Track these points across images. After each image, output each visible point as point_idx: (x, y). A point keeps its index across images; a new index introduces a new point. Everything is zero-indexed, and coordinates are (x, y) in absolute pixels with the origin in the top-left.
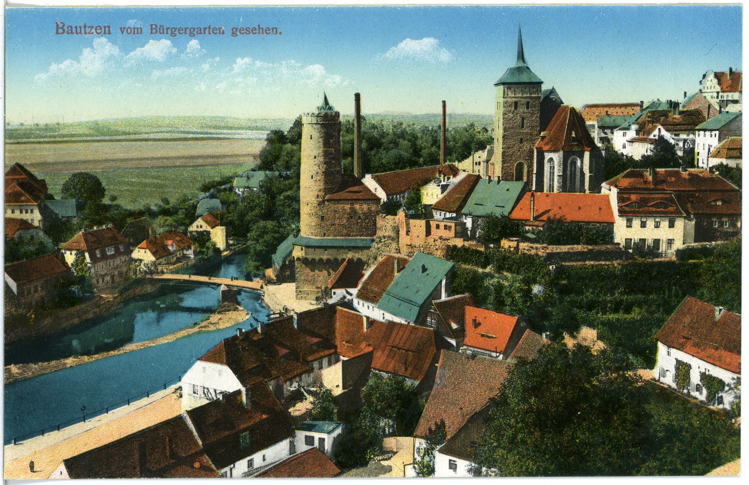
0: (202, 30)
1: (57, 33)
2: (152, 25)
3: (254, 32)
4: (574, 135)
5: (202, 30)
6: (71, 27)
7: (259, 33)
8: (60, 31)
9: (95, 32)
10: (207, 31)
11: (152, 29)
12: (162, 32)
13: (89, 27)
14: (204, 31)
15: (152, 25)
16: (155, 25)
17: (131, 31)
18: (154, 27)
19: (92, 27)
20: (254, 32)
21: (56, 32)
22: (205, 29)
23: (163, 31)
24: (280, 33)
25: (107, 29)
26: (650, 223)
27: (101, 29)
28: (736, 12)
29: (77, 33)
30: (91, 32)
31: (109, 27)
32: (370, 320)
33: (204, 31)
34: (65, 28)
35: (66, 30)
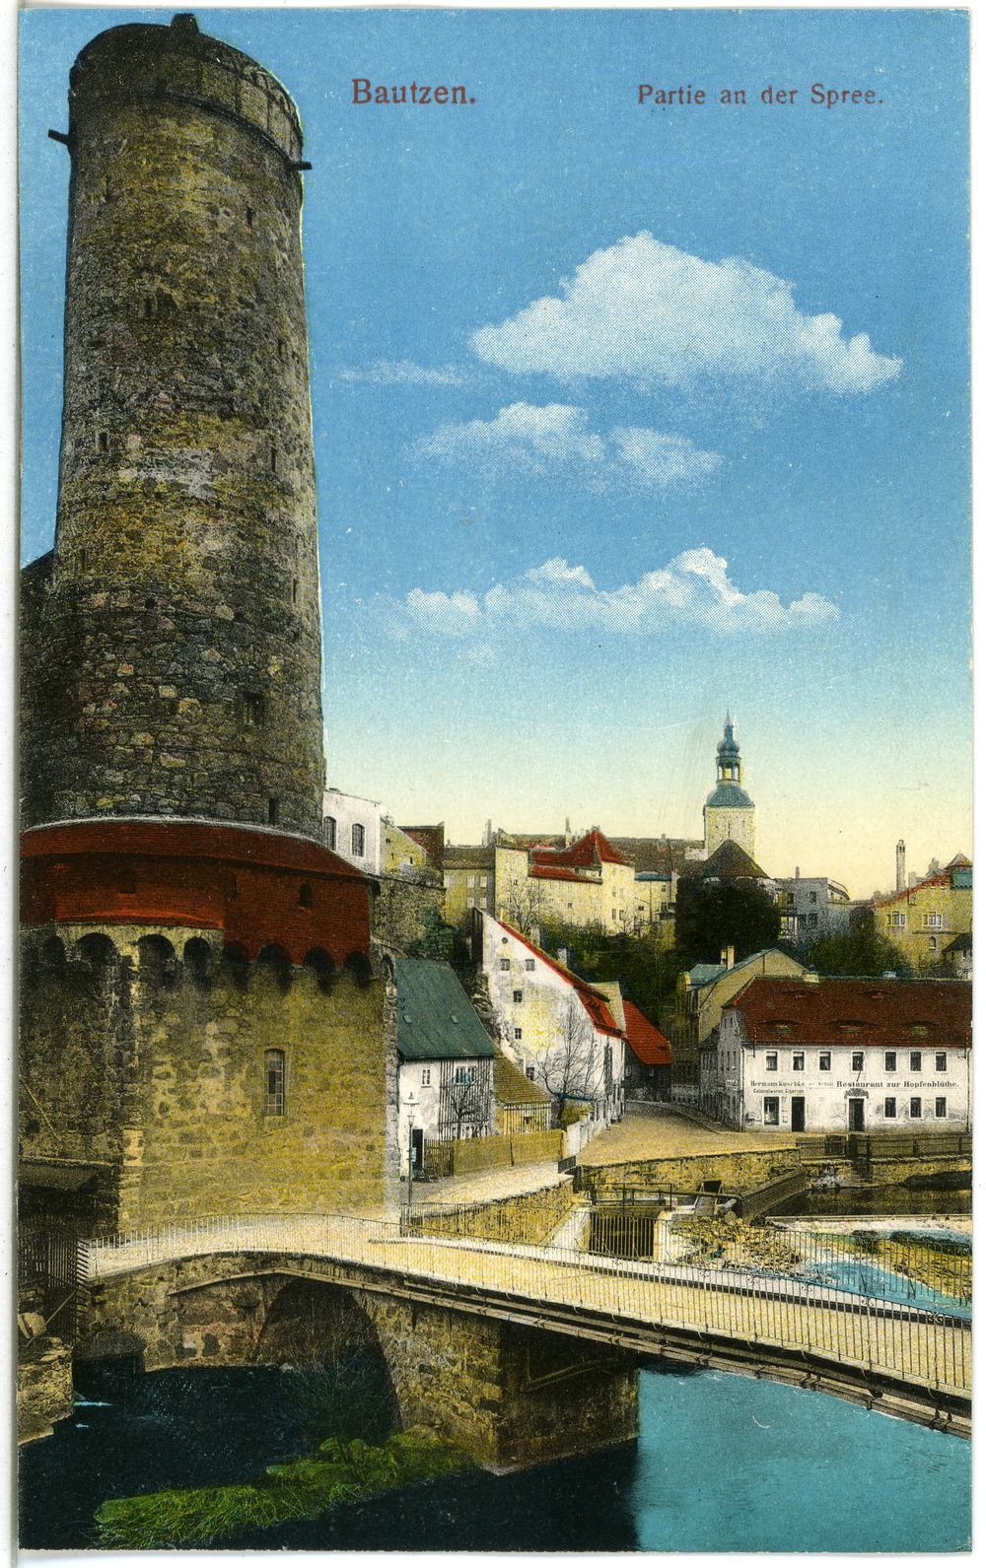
0: (667, 97)
1: (356, 101)
2: (356, 81)
3: (442, 97)
4: (350, 530)
5: (667, 97)
6: (384, 89)
7: (455, 101)
8: (362, 96)
9: (433, 98)
10: (676, 96)
11: (356, 91)
12: (399, 97)
13: (421, 89)
14: (671, 97)
15: (356, 81)
16: (647, 86)
17: (837, 98)
18: (362, 86)
19: (428, 89)
20: (442, 97)
21: (353, 99)
22: (671, 93)
23: (404, 95)
24: (472, 101)
25: (459, 93)
26: (786, 1057)
27: (446, 93)
28: (957, 22)
29: (396, 101)
30: (427, 99)
31: (743, 93)
32: (960, 957)
33: (671, 97)
34: (372, 90)
35: (374, 95)
